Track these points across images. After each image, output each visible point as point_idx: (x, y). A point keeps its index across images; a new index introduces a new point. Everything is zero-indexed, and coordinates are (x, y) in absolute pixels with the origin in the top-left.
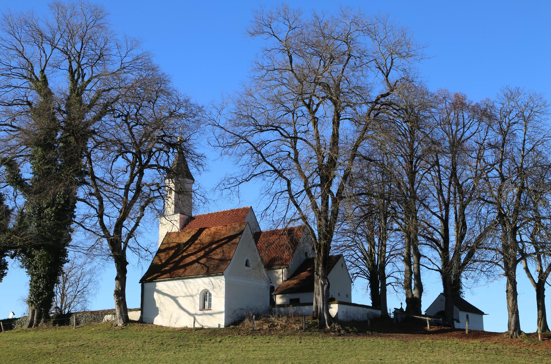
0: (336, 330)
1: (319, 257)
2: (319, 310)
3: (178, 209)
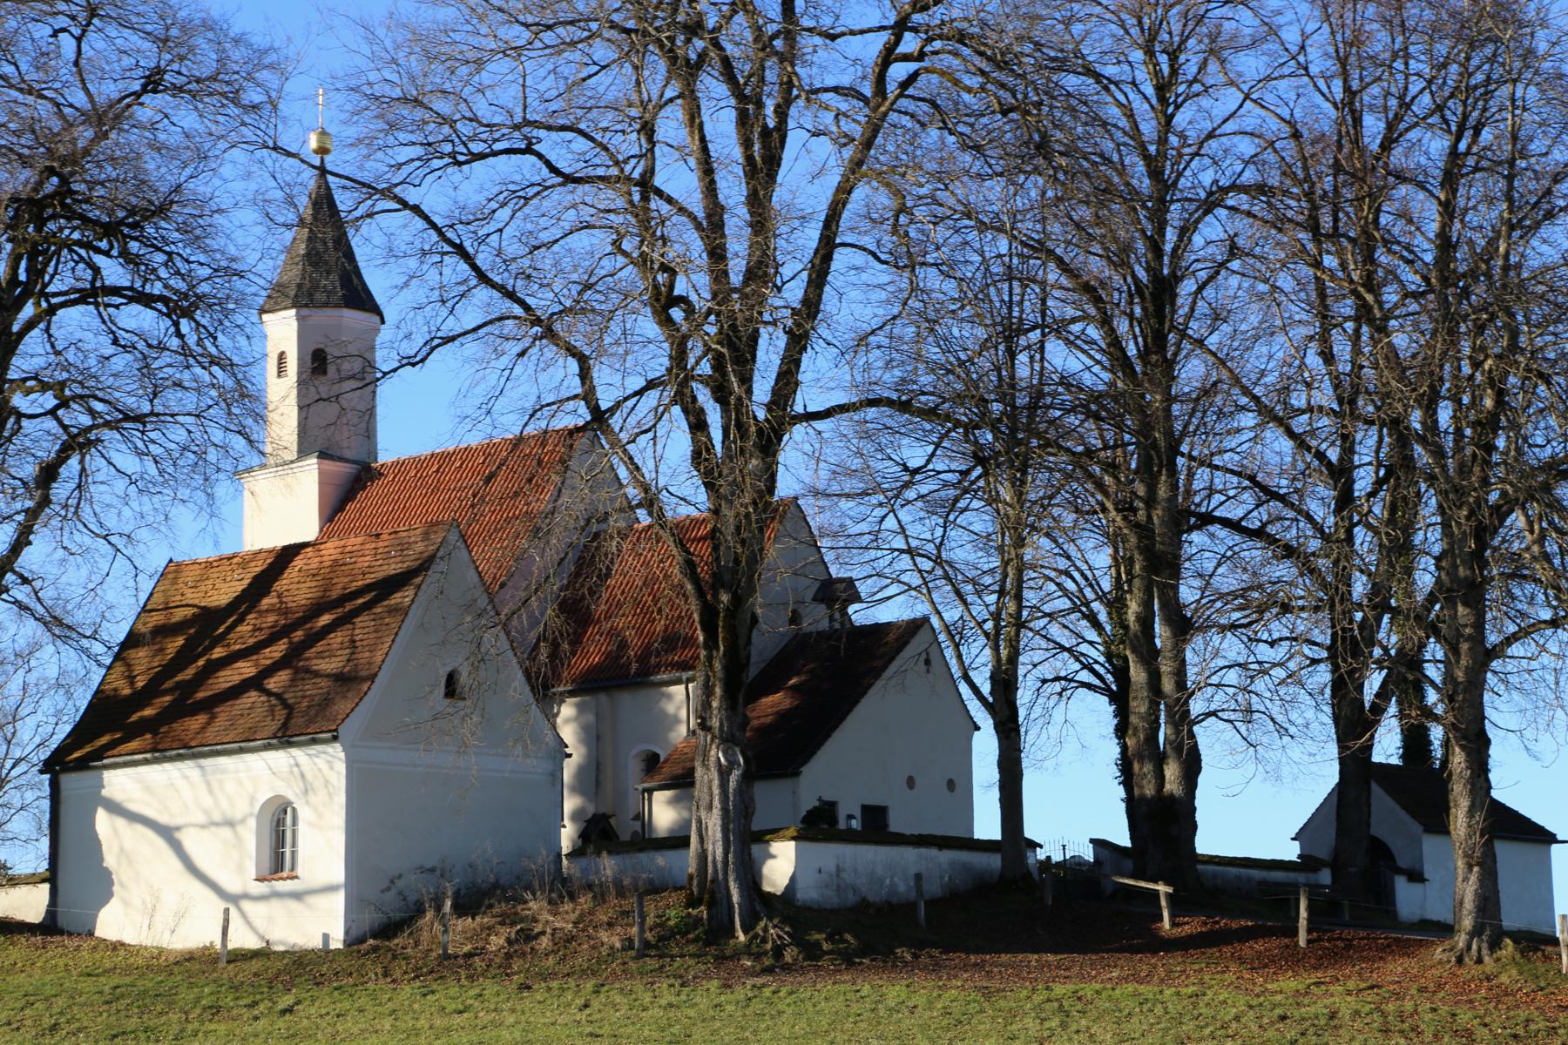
0: (769, 946)
1: (710, 658)
2: (710, 870)
3: (314, 441)
